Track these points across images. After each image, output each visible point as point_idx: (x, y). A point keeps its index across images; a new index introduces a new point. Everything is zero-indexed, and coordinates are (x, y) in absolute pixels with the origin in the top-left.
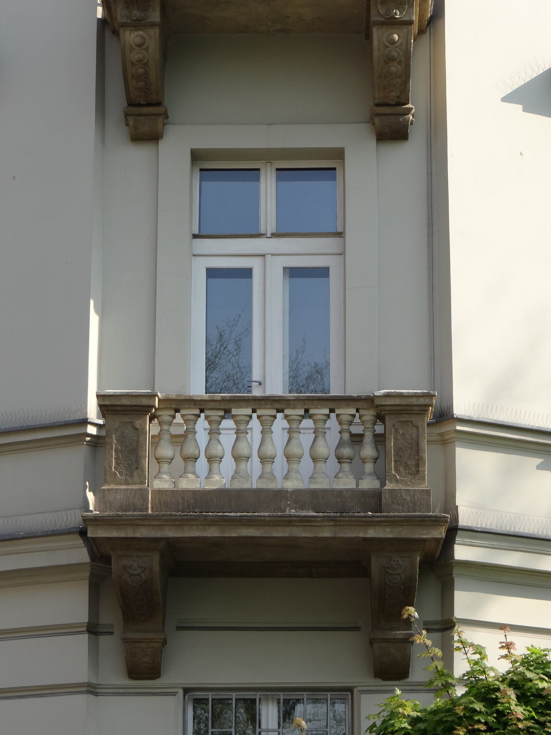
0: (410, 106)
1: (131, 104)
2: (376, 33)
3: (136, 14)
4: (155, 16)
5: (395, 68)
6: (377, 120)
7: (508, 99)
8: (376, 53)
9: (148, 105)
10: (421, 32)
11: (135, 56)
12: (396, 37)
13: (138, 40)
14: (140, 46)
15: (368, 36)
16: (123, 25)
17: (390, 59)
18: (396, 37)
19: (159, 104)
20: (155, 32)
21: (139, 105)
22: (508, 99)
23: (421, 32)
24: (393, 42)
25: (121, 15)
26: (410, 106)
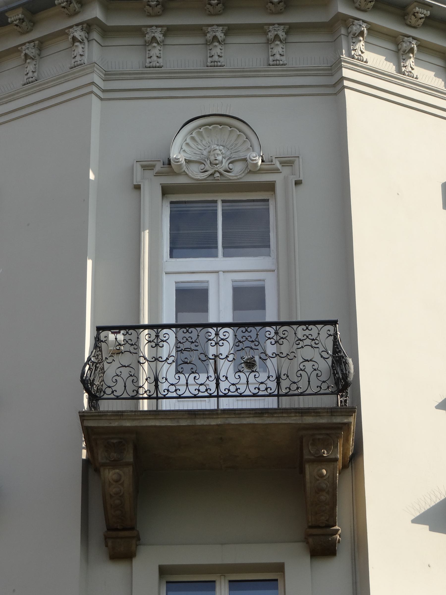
0: (337, 527)
1: (109, 529)
2: (308, 468)
3: (114, 455)
4: (129, 457)
5: (324, 497)
6: (310, 540)
7: (417, 520)
8: (308, 485)
9: (124, 529)
10: (345, 467)
11: (113, 490)
12: (324, 472)
13: (115, 477)
14: (117, 481)
15: (302, 471)
16: (104, 465)
17: (320, 490)
18: (324, 472)
19: (132, 528)
20: (129, 470)
21: (117, 530)
22: (417, 520)
23: (345, 467)
24: (322, 476)
25: (101, 457)
26: (337, 527)
